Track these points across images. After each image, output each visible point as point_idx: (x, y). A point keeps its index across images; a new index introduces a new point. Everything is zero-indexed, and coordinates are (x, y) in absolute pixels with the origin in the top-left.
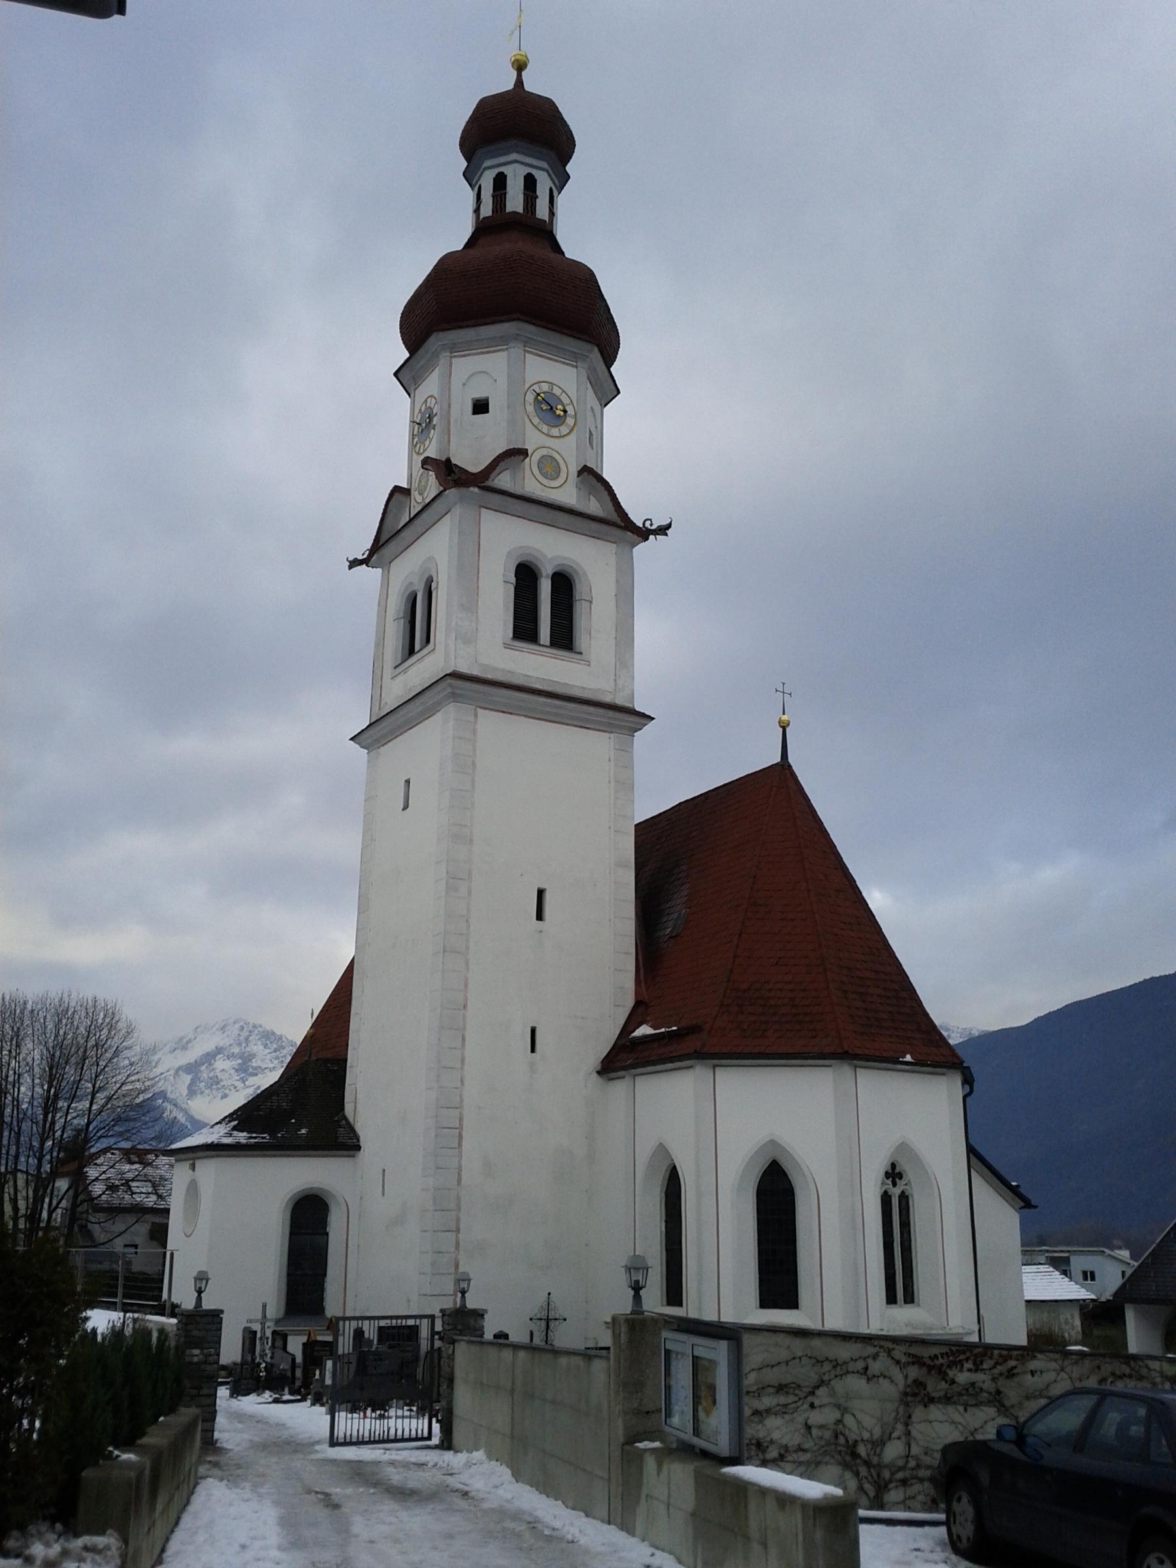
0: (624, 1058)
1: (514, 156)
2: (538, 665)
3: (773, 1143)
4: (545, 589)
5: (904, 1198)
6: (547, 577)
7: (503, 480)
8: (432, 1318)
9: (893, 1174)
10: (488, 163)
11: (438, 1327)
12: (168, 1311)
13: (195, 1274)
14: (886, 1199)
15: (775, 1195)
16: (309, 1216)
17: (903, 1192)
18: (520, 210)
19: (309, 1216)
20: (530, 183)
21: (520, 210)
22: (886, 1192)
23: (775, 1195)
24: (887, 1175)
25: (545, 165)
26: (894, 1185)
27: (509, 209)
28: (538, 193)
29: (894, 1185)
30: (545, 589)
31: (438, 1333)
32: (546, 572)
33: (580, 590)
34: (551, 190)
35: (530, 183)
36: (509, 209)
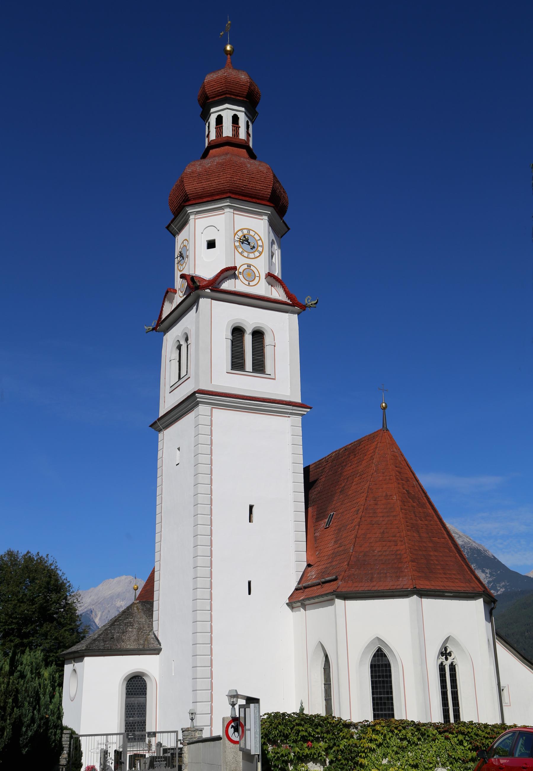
0: (305, 595)
1: (227, 106)
2: (246, 383)
3: (378, 639)
4: (248, 340)
5: (453, 668)
6: (249, 334)
7: (227, 285)
8: (176, 732)
9: (445, 653)
10: (212, 110)
11: (180, 737)
12: (136, 700)
13: (288, 609)
14: (442, 668)
15: (381, 670)
16: (136, 685)
17: (452, 663)
18: (230, 135)
19: (136, 685)
20: (235, 119)
21: (230, 135)
22: (442, 663)
23: (381, 670)
24: (442, 654)
25: (243, 109)
26: (447, 659)
27: (225, 135)
28: (240, 125)
29: (447, 659)
30: (248, 340)
31: (180, 740)
32: (249, 331)
33: (268, 340)
34: (247, 122)
35: (235, 119)
36: (225, 135)
